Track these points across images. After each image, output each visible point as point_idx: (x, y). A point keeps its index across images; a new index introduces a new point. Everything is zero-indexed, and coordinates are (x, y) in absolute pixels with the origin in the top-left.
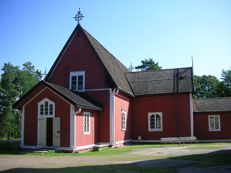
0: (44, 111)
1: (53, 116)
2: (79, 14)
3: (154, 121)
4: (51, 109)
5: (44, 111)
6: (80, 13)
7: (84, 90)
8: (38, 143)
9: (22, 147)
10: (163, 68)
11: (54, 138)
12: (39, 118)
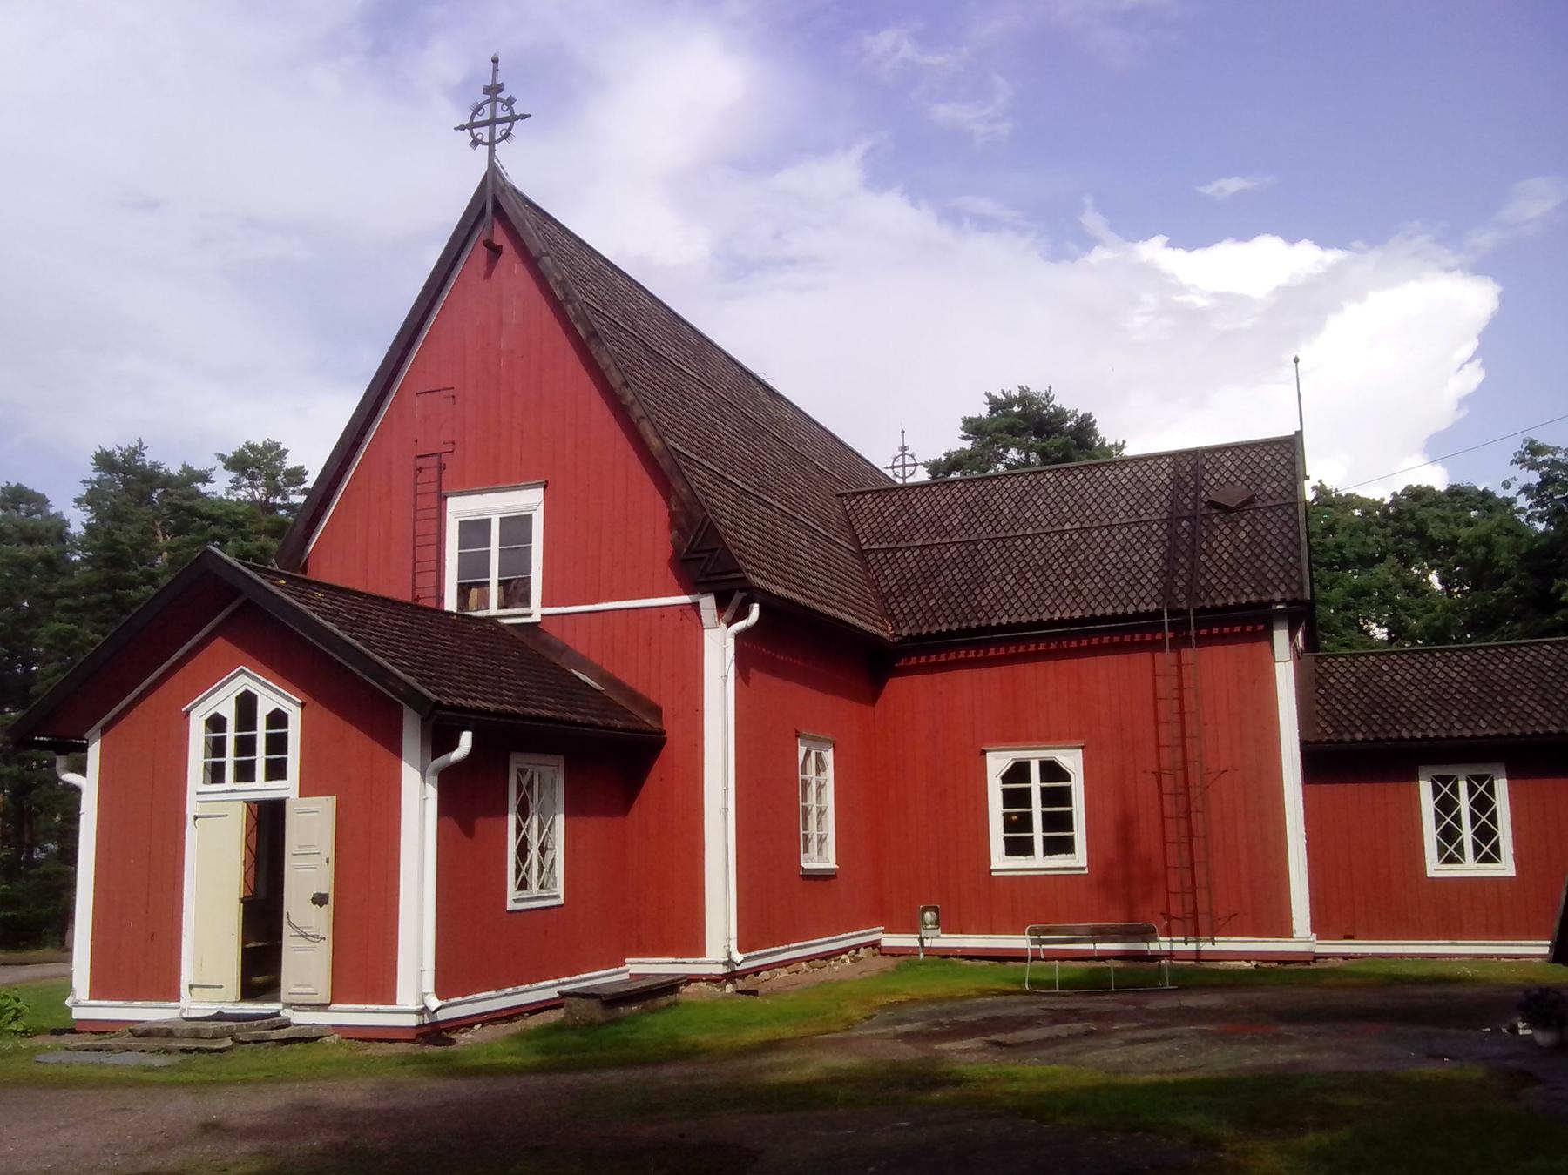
0: (230, 759)
1: (288, 788)
2: (904, 455)
3: (1043, 789)
4: (277, 744)
5: (230, 759)
6: (503, 96)
7: (536, 611)
8: (187, 976)
9: (78, 1014)
10: (1130, 451)
11: (290, 943)
12: (192, 808)
